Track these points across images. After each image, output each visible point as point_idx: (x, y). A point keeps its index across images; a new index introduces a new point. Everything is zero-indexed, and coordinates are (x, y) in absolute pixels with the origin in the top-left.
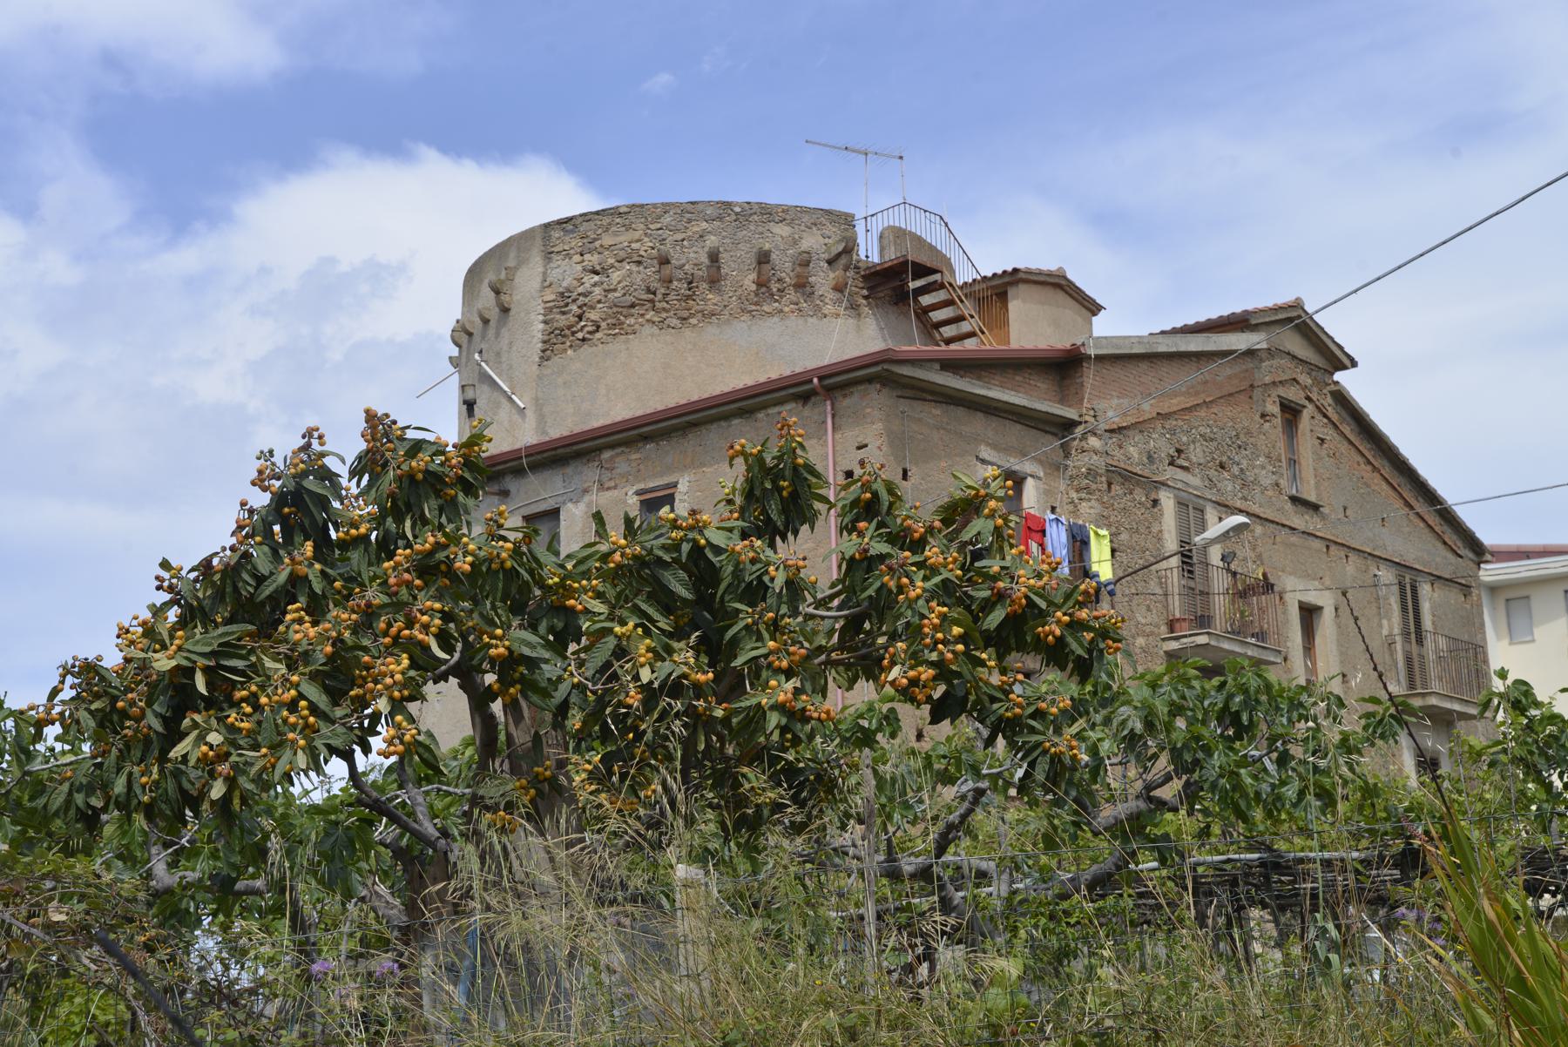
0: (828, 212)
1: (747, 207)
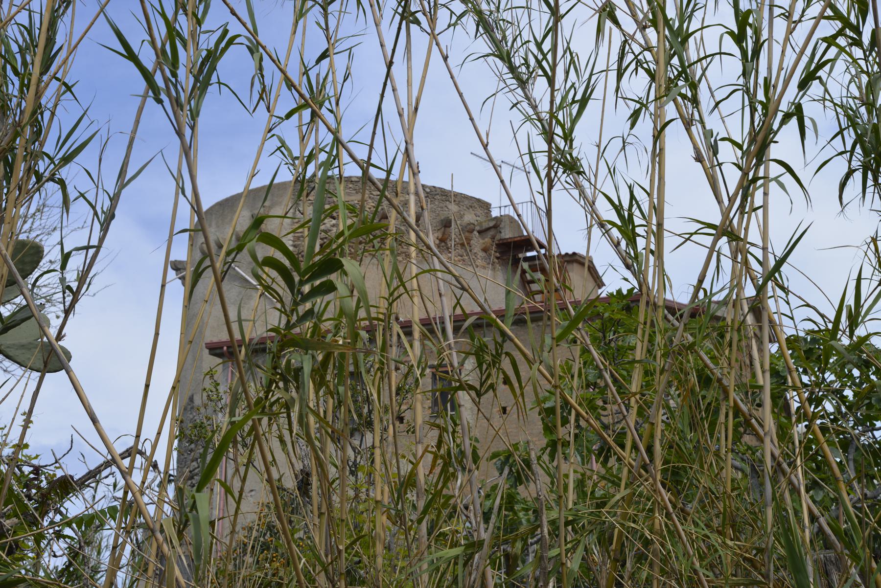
0: (479, 200)
1: (433, 190)
